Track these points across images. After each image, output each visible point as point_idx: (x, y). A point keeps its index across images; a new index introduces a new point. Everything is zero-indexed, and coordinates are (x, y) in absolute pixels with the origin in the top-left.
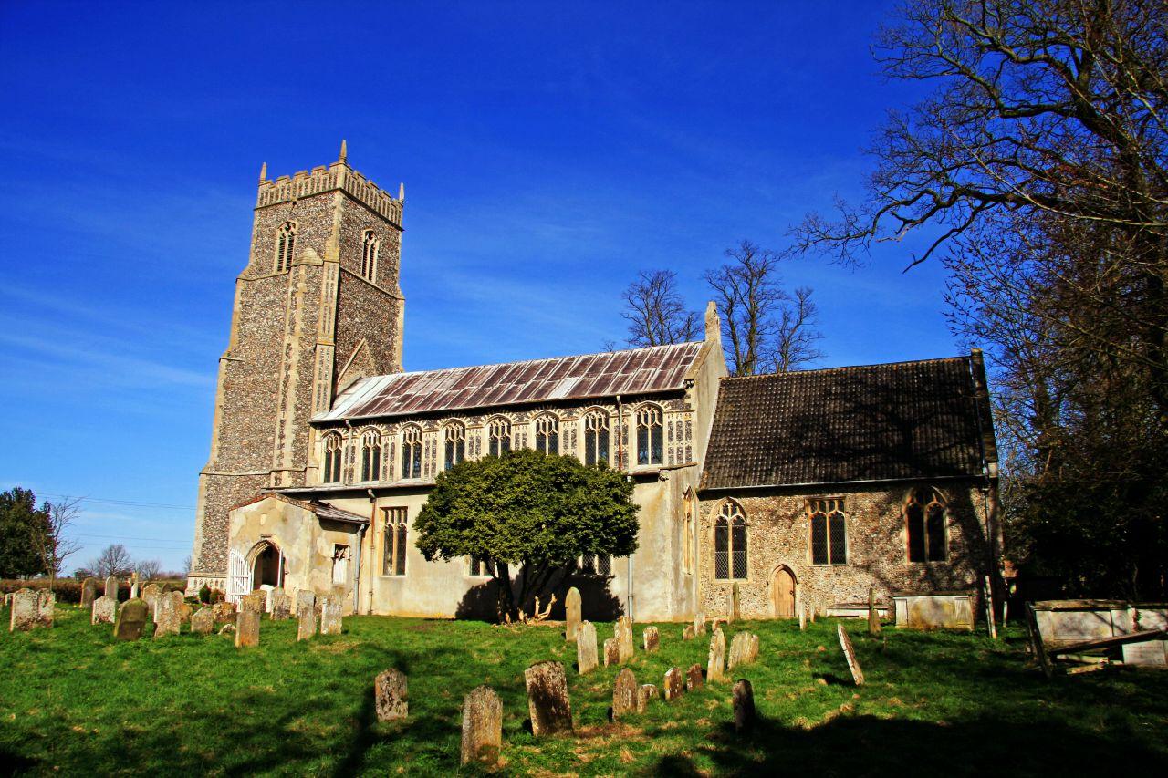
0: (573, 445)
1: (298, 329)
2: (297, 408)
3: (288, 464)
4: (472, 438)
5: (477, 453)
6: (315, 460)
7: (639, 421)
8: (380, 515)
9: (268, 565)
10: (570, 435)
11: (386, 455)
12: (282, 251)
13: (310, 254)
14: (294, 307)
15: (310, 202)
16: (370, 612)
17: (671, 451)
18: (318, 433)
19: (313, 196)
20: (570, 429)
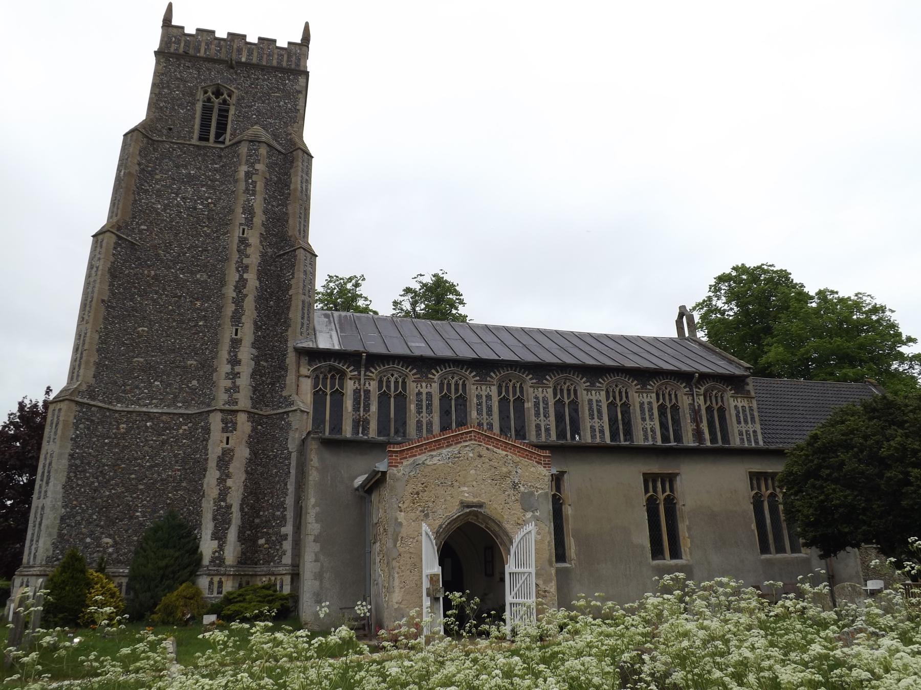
3: (244, 400)
4: (536, 398)
5: (545, 416)
10: (646, 406)
15: (259, 73)
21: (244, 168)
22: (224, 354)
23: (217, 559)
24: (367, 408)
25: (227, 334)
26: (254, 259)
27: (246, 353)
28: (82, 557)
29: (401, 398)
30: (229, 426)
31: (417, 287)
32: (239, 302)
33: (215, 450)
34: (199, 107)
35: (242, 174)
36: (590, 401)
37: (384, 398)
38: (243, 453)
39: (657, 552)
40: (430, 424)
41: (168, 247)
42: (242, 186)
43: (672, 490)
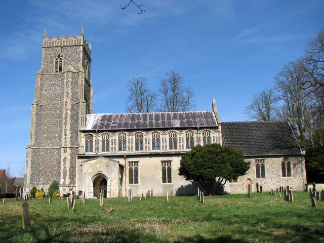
0: (183, 142)
1: (70, 95)
2: (71, 125)
3: (69, 145)
6: (82, 144)
7: (152, 137)
8: (127, 164)
9: (100, 182)
10: (181, 139)
11: (112, 143)
12: (56, 65)
14: (67, 87)
15: (69, 48)
16: (126, 196)
17: (163, 146)
18: (83, 135)
19: (71, 46)
20: (181, 137)
21: (66, 80)
22: (63, 133)
23: (64, 183)
24: (98, 144)
25: (64, 127)
26: (69, 106)
27: (68, 132)
29: (108, 141)
30: (65, 151)
31: (181, 79)
32: (66, 119)
33: (62, 158)
34: (54, 62)
35: (65, 83)
36: (163, 138)
37: (103, 141)
38: (69, 158)
39: (164, 181)
40: (115, 148)
41: (49, 105)
42: (65, 86)
43: (170, 165)
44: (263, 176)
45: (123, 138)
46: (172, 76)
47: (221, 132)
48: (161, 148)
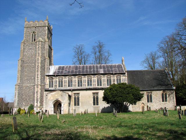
0: (105, 82)
1: (40, 55)
2: (41, 72)
3: (39, 83)
6: (47, 83)
7: (88, 79)
8: (73, 94)
9: (58, 105)
10: (104, 80)
11: (64, 82)
12: (32, 37)
13: (40, 39)
14: (39, 50)
15: (40, 27)
17: (94, 84)
18: (47, 78)
19: (40, 27)
20: (104, 79)
21: (38, 46)
22: (36, 77)
23: (37, 106)
24: (56, 83)
25: (37, 73)
26: (40, 61)
27: (39, 76)
28: (157, 136)
29: (62, 81)
30: (38, 87)
32: (38, 68)
33: (36, 91)
34: (31, 35)
35: (37, 48)
36: (93, 80)
37: (59, 81)
38: (40, 91)
39: (94, 104)
40: (66, 85)
41: (28, 60)
42: (37, 49)
43: (98, 95)
44: (151, 101)
45: (71, 79)
46: (99, 44)
47: (127, 76)
48: (93, 85)
